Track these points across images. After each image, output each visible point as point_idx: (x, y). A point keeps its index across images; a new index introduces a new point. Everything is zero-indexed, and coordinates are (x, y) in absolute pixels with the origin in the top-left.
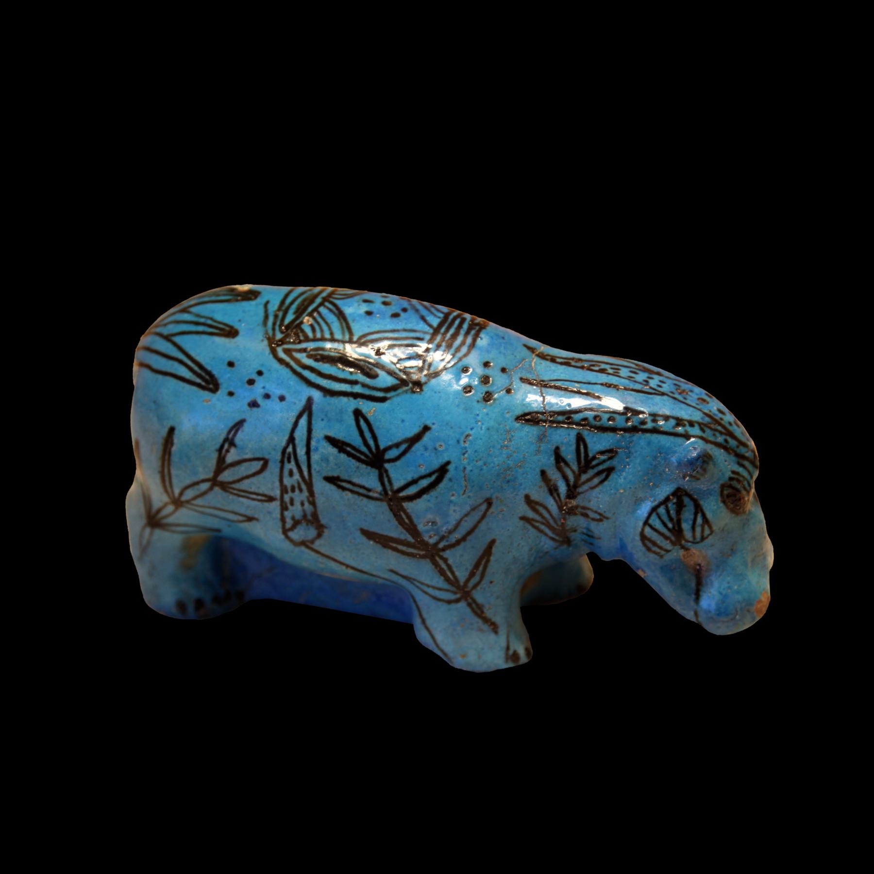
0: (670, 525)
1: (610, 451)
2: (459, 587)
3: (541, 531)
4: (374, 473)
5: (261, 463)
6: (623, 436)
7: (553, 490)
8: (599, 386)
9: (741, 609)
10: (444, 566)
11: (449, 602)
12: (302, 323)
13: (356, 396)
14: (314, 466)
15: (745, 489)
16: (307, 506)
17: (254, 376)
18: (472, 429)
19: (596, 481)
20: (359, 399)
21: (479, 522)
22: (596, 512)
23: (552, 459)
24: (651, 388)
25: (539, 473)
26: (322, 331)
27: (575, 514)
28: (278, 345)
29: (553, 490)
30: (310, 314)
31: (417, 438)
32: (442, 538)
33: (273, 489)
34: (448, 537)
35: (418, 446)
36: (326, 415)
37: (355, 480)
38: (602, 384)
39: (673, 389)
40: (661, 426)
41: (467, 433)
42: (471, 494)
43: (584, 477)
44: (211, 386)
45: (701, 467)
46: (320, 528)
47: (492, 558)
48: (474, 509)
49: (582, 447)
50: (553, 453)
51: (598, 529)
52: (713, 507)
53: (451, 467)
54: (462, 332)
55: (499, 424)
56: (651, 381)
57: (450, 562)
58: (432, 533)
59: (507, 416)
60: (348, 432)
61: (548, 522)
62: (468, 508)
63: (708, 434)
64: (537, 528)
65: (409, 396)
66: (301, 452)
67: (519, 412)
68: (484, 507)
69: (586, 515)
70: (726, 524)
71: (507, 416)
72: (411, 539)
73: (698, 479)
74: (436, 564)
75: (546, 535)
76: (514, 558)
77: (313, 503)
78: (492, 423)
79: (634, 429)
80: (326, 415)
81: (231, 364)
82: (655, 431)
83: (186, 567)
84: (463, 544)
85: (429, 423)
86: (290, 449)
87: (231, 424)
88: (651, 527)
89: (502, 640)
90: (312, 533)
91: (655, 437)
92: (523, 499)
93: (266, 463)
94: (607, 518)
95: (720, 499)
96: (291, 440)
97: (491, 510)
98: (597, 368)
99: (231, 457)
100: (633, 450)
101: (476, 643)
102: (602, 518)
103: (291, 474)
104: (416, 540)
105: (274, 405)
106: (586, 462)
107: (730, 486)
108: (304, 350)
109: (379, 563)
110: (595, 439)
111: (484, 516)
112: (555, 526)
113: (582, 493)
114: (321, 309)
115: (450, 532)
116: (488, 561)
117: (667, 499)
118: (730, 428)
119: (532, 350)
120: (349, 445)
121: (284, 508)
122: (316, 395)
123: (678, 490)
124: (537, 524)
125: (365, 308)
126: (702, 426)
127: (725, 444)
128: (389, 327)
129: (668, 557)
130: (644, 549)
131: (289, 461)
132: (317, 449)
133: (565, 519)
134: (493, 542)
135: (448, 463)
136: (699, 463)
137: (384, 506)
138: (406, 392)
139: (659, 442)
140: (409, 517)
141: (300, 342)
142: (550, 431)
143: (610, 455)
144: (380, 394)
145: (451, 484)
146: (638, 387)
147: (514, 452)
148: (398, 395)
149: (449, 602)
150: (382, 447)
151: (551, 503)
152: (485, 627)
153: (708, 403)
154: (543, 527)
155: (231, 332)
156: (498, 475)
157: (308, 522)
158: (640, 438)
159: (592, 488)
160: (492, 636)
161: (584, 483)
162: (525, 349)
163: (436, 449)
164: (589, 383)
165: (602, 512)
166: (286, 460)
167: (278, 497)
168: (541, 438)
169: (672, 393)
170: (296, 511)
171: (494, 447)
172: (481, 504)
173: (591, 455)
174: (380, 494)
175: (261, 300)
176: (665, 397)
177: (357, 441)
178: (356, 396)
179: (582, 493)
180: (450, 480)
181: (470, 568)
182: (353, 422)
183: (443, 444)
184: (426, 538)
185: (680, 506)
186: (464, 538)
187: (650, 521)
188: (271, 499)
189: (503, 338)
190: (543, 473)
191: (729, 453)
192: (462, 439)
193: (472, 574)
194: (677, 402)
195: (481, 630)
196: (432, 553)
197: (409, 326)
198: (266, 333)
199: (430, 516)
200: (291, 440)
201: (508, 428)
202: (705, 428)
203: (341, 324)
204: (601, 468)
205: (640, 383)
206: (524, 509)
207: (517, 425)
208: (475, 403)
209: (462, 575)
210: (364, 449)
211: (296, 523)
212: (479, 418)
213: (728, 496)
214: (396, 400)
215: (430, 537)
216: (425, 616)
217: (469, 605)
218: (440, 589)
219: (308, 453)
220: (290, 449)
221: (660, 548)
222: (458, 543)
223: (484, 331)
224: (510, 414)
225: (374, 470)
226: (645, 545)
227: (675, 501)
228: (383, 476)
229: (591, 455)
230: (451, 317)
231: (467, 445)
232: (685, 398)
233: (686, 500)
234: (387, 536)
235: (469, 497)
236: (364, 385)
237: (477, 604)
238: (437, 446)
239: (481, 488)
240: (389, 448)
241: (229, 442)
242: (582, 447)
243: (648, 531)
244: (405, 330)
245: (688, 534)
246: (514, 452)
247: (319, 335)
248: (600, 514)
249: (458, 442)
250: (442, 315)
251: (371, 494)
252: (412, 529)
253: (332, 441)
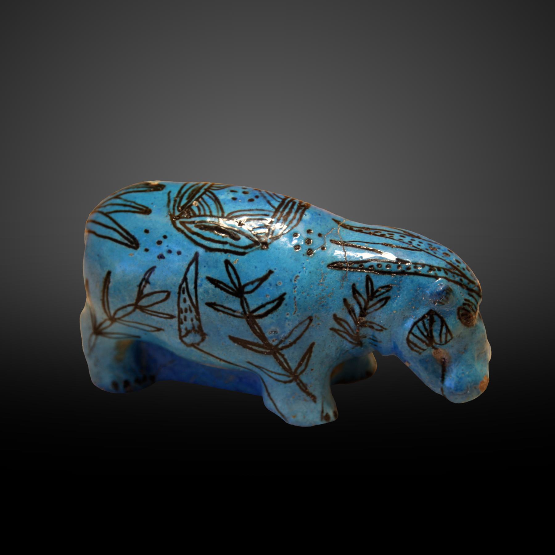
0: (426, 334)
1: (387, 286)
2: (291, 373)
3: (344, 337)
4: (237, 301)
5: (166, 294)
6: (395, 277)
7: (351, 311)
8: (381, 245)
9: (471, 387)
10: (282, 360)
11: (285, 382)
12: (192, 205)
13: (226, 251)
14: (200, 296)
15: (473, 310)
16: (195, 321)
17: (162, 239)
18: (299, 272)
19: (379, 305)
20: (228, 254)
21: (304, 331)
22: (378, 325)
23: (351, 291)
24: (413, 246)
25: (342, 301)
26: (204, 210)
27: (365, 326)
28: (177, 219)
29: (351, 311)
30: (197, 200)
31: (265, 278)
32: (281, 342)
33: (173, 311)
34: (284, 341)
35: (265, 283)
36: (207, 264)
37: (226, 305)
38: (382, 244)
39: (427, 247)
40: (420, 271)
41: (296, 275)
42: (299, 314)
43: (371, 303)
44: (134, 245)
45: (445, 297)
46: (203, 336)
47: (312, 354)
48: (301, 323)
49: (369, 284)
50: (351, 287)
51: (380, 336)
52: (453, 322)
53: (286, 297)
54: (294, 211)
55: (317, 270)
56: (413, 242)
57: (286, 357)
58: (274, 339)
59: (322, 264)
60: (221, 274)
61: (348, 332)
62: (297, 323)
63: (450, 276)
64: (341, 335)
65: (259, 251)
66: (191, 287)
67: (329, 262)
68: (307, 322)
69: (372, 327)
70: (461, 333)
71: (322, 264)
72: (261, 342)
73: (443, 304)
74: (277, 358)
75: (347, 339)
76: (327, 354)
77: (199, 320)
78: (312, 269)
79: (403, 273)
80: (207, 264)
81: (147, 231)
82: (416, 274)
83: (118, 360)
84: (294, 346)
85: (272, 269)
86: (184, 285)
87: (147, 269)
88: (413, 334)
89: (319, 407)
90: (198, 338)
91: (416, 278)
92: (332, 317)
93: (169, 294)
94: (386, 329)
95: (457, 317)
96: (185, 279)
97: (312, 324)
98: (379, 234)
99: (147, 290)
100: (402, 286)
101: (302, 409)
102: (382, 329)
103: (185, 301)
104: (264, 343)
105: (174, 257)
106: (372, 293)
107: (464, 309)
108: (193, 222)
109: (241, 358)
110: (378, 279)
111: (307, 328)
112: (353, 334)
113: (369, 313)
114: (204, 196)
115: (286, 338)
116: (310, 356)
117: (424, 317)
118: (464, 272)
119: (338, 222)
120: (222, 283)
121: (180, 322)
122: (201, 251)
123: (431, 311)
124: (341, 333)
125: (232, 195)
126: (446, 271)
127: (460, 282)
128: (247, 208)
129: (424, 354)
130: (409, 349)
131: (184, 293)
132: (201, 285)
133: (358, 329)
134: (313, 344)
135: (285, 294)
136: (444, 294)
137: (244, 322)
138: (258, 249)
139: (419, 280)
140: (260, 328)
141: (191, 217)
142: (349, 274)
143: (387, 289)
144: (241, 250)
145: (286, 307)
146: (405, 246)
147: (327, 287)
148: (253, 251)
149: (285, 382)
150: (242, 284)
151: (350, 320)
152: (308, 398)
153: (449, 256)
154: (345, 335)
155: (147, 211)
156: (316, 302)
157: (196, 331)
158: (406, 278)
159: (376, 310)
160: (313, 404)
161: (371, 307)
163: (277, 285)
164: (374, 243)
165: (382, 325)
166: (181, 292)
167: (177, 315)
168: (344, 278)
169: (427, 249)
170: (188, 324)
171: (313, 284)
172: (305, 320)
173: (375, 289)
174: (242, 314)
175: (166, 191)
176: (422, 252)
177: (227, 280)
178: (226, 251)
179: (369, 313)
180: (286, 305)
181: (299, 361)
182: (224, 268)
183: (281, 282)
184: (271, 342)
185: (432, 322)
186: (295, 342)
187: (413, 331)
188: (172, 317)
189: (320, 215)
190: (345, 300)
191: (463, 288)
192: (294, 279)
193: (300, 365)
194: (430, 255)
195: (305, 400)
196: (274, 351)
197: (260, 207)
198: (169, 211)
199: (273, 328)
200: (185, 279)
201: (322, 271)
202: (448, 272)
203: (217, 206)
204: (382, 297)
205: (407, 243)
206: (333, 323)
207: (329, 270)
208: (302, 256)
209: (293, 365)
210: (231, 285)
211: (188, 332)
212: (304, 265)
213: (463, 315)
214: (251, 254)
215: (273, 341)
216: (270, 391)
217: (298, 384)
218: (279, 374)
219: (196, 288)
220: (184, 285)
221: (419, 348)
222: (291, 345)
223: (307, 210)
224: (324, 263)
225: (237, 298)
226: (409, 346)
227: (428, 318)
228: (243, 302)
229: (375, 289)
230: (287, 201)
231: (296, 283)
232: (435, 253)
233: (436, 318)
234: (245, 341)
235: (298, 316)
236: (231, 245)
237: (303, 384)
238: (278, 283)
239: (305, 310)
240: (247, 284)
241: (146, 280)
242: (369, 284)
244: (257, 210)
245: (437, 339)
246: (327, 287)
247: (202, 213)
248: (381, 327)
249: (291, 280)
250: (280, 200)
251: (236, 314)
252: (262, 336)
253: (211, 280)
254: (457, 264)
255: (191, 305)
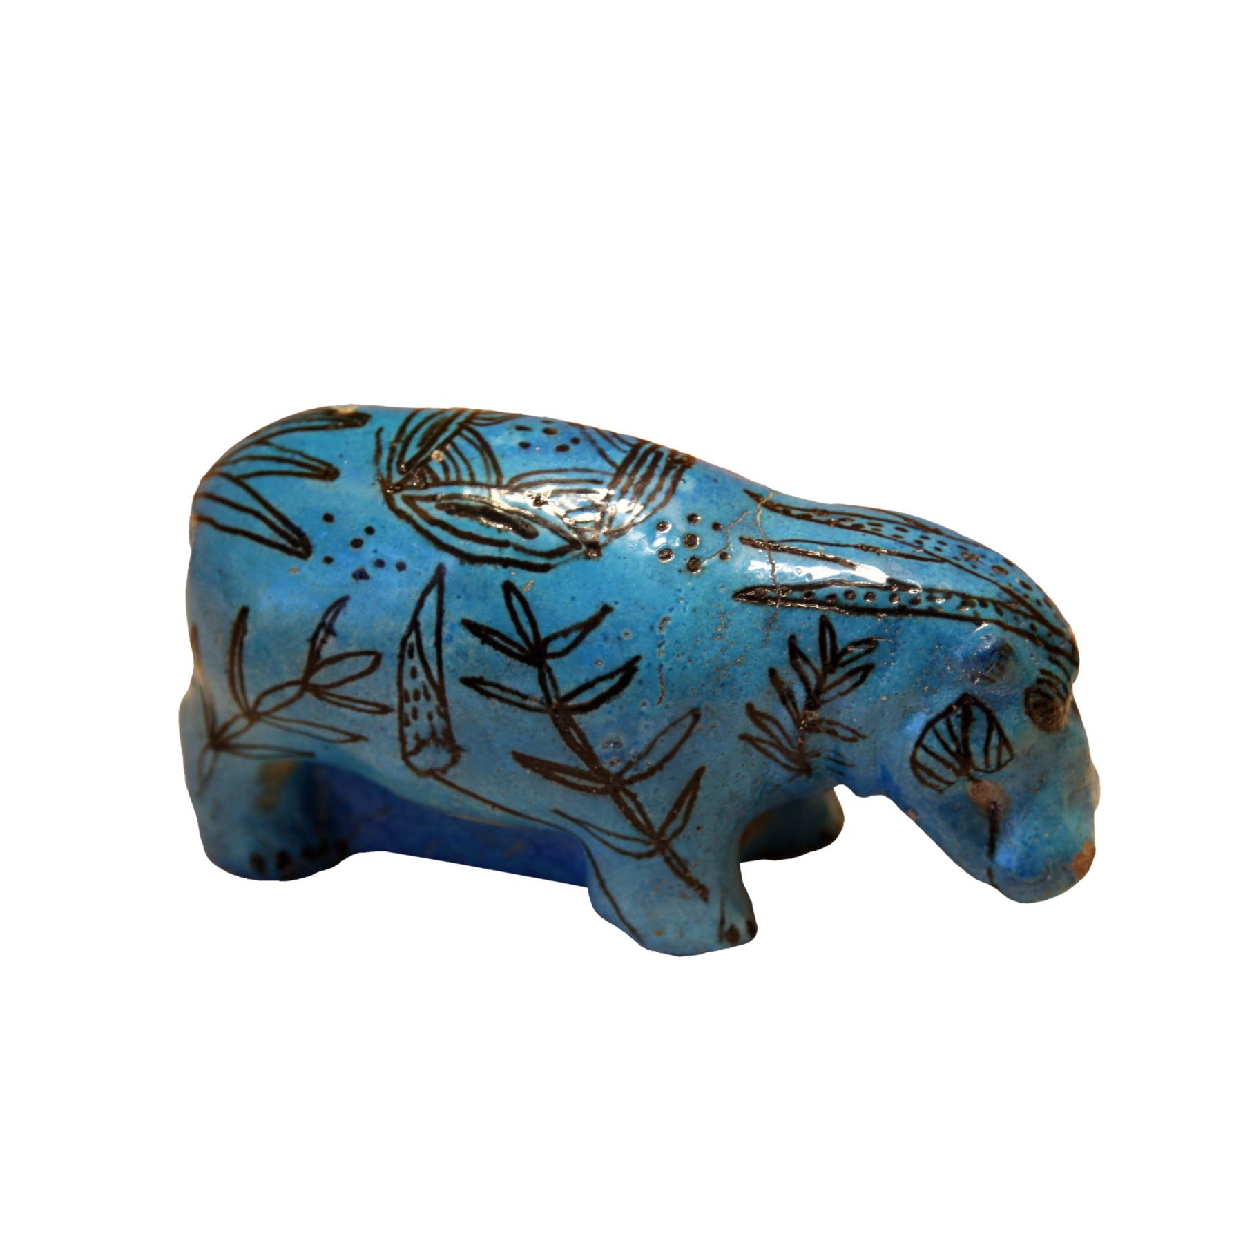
0: (953, 747)
1: (868, 641)
2: (652, 835)
3: (770, 756)
4: (532, 673)
5: (372, 658)
6: (886, 620)
7: (786, 697)
8: (853, 549)
9: (1054, 866)
10: (631, 805)
11: (639, 856)
12: (429, 459)
13: (506, 563)
14: (447, 663)
15: (1059, 695)
16: (436, 719)
17: (362, 535)
18: (671, 610)
19: (848, 683)
20: (510, 568)
21: (682, 742)
22: (847, 728)
23: (786, 652)
24: (926, 552)
25: (767, 673)
26: (458, 470)
27: (818, 731)
28: (396, 491)
29: (786, 697)
30: (441, 447)
31: (594, 623)
32: (629, 765)
33: (388, 696)
34: (637, 763)
35: (594, 635)
36: (464, 591)
37: (505, 683)
38: (856, 547)
39: (957, 553)
40: (940, 606)
41: (664, 616)
42: (670, 703)
43: (831, 679)
44: (300, 549)
45: (997, 664)
46: (456, 752)
47: (700, 794)
48: (674, 724)
49: (827, 635)
50: (786, 644)
52: (1014, 721)
53: (641, 665)
54: (658, 472)
55: (710, 604)
56: (925, 542)
57: (640, 799)
58: (614, 758)
59: (722, 591)
60: (494, 614)
61: (779, 743)
62: (666, 723)
63: (1007, 617)
64: (763, 751)
65: (581, 563)
66: (428, 642)
67: (738, 586)
68: (688, 721)
69: (833, 733)
70: (1033, 746)
71: (722, 591)
72: (584, 767)
73: (993, 681)
74: (620, 802)
75: (776, 760)
76: (731, 793)
77: (445, 716)
78: (699, 602)
79: (902, 611)
80: (464, 591)
81: (328, 518)
82: (932, 613)
83: (264, 806)
84: (658, 774)
85: (610, 602)
86: (412, 639)
87: (328, 603)
88: (926, 749)
89: (714, 910)
90: (444, 757)
91: (931, 622)
92: (744, 710)
93: (378, 658)
94: (864, 737)
95: (1023, 709)
96: (414, 625)
97: (699, 726)
98: (849, 524)
99: (329, 650)
100: (900, 641)
102: (856, 736)
103: (414, 674)
104: (592, 768)
105: (389, 575)
106: (833, 657)
107: (1039, 692)
108: (433, 498)
110: (846, 624)
111: (688, 734)
112: (790, 748)
113: (827, 701)
115: (641, 757)
116: (694, 798)
117: (949, 710)
118: (1038, 609)
120: (496, 633)
121: (404, 722)
122: (450, 561)
123: (965, 696)
124: (764, 746)
125: (518, 437)
126: (999, 606)
127: (1031, 631)
128: (554, 465)
129: (950, 792)
130: (915, 781)
131: (411, 656)
132: (450, 639)
133: (803, 738)
134: (701, 771)
135: (638, 658)
136: (994, 659)
137: (546, 720)
138: (577, 557)
139: (937, 628)
140: (582, 735)
141: (427, 486)
142: (782, 613)
143: (867, 647)
144: (541, 561)
145: (641, 688)
146: (907, 550)
147: (732, 643)
148: (566, 562)
149: (639, 856)
150: (543, 635)
151: (784, 716)
152: (690, 892)
153: (1007, 573)
154: (772, 750)
155: (328, 473)
156: (708, 676)
157: (439, 742)
158: (910, 623)
159: (842, 694)
160: (700, 905)
161: (831, 687)
162: (746, 496)
163: (619, 638)
164: (838, 545)
165: (856, 728)
166: (406, 654)
167: (396, 706)
168: (769, 623)
169: (956, 558)
170: (420, 726)
171: (702, 635)
172: (684, 717)
173: (840, 647)
174: (541, 702)
175: (371, 427)
176: (946, 565)
177: (508, 628)
178: (506, 563)
179: (827, 701)
180: (641, 682)
181: (669, 807)
182: (501, 601)
183: (629, 631)
184: (606, 766)
185: (967, 720)
186: (660, 766)
187: (925, 742)
188: (385, 710)
189: (716, 481)
190: (772, 673)
191: (1037, 645)
192: (657, 624)
193: (671, 817)
194: (962, 571)
195: (683, 896)
196: (615, 787)
197: (582, 464)
198: (379, 473)
199: (611, 734)
200: (414, 625)
201: (722, 608)
202: (1003, 609)
203: (485, 461)
204: (855, 665)
205: (911, 545)
206: (746, 724)
207: (736, 604)
208: (676, 573)
209: (657, 818)
210: (517, 638)
211: (421, 744)
212: (681, 594)
213: (1036, 705)
214: (563, 569)
215: (612, 764)
216: (604, 875)
217: (667, 860)
218: (626, 838)
219: (438, 644)
220: (412, 639)
221: (939, 779)
222: (651, 772)
223: (688, 470)
224: (726, 589)
225: (531, 668)
226: (917, 775)
227: (960, 712)
228: (545, 676)
229: (840, 647)
230: (642, 451)
231: (664, 633)
232: (974, 567)
233: (976, 711)
234: (550, 763)
235: (667, 707)
236: (518, 548)
237: (679, 860)
238: (622, 634)
239: (684, 694)
240: (554, 637)
241: (326, 628)
242: (827, 635)
243: (921, 755)
244: (576, 470)
245: (978, 760)
246: (732, 643)
247: (453, 477)
248: (853, 731)
249: (652, 628)
250: (628, 449)
251: (528, 702)
252: (586, 752)
253: (473, 627)
254: (1024, 591)
255: (427, 683)
